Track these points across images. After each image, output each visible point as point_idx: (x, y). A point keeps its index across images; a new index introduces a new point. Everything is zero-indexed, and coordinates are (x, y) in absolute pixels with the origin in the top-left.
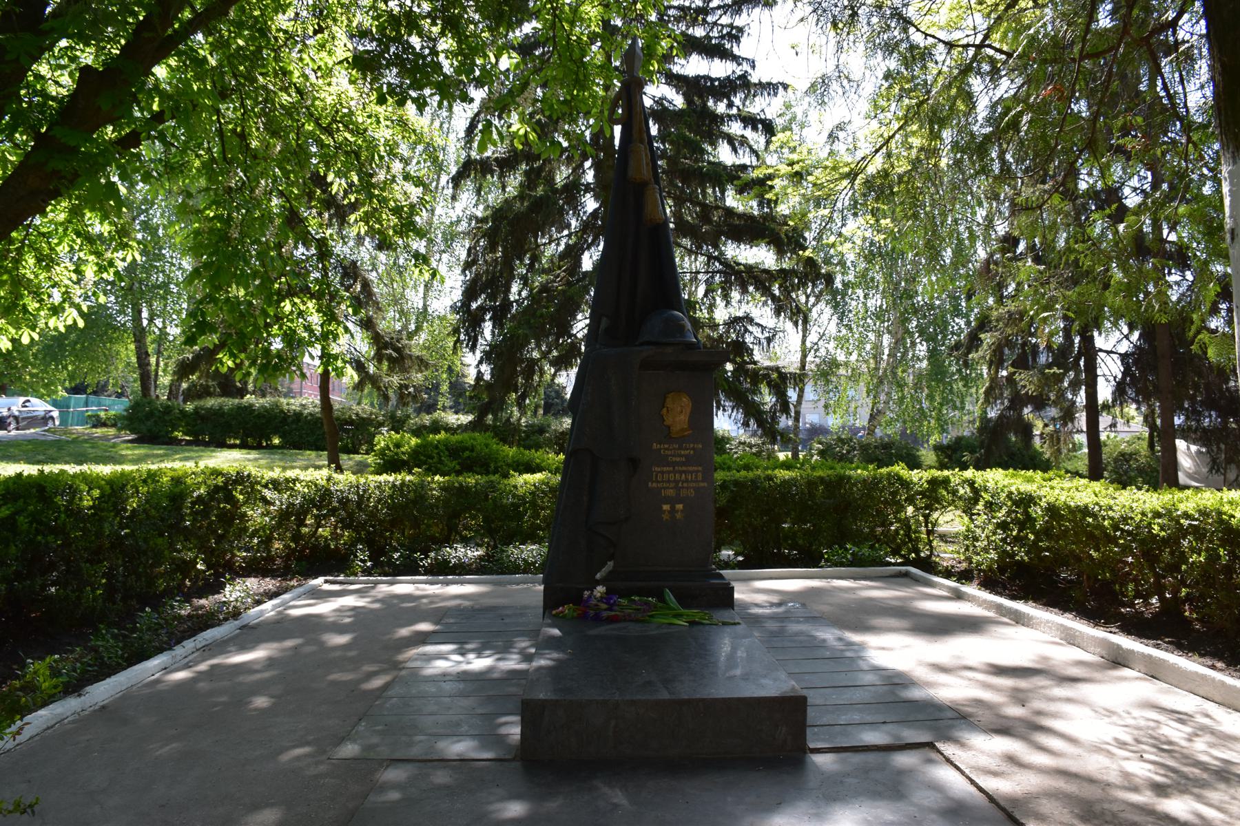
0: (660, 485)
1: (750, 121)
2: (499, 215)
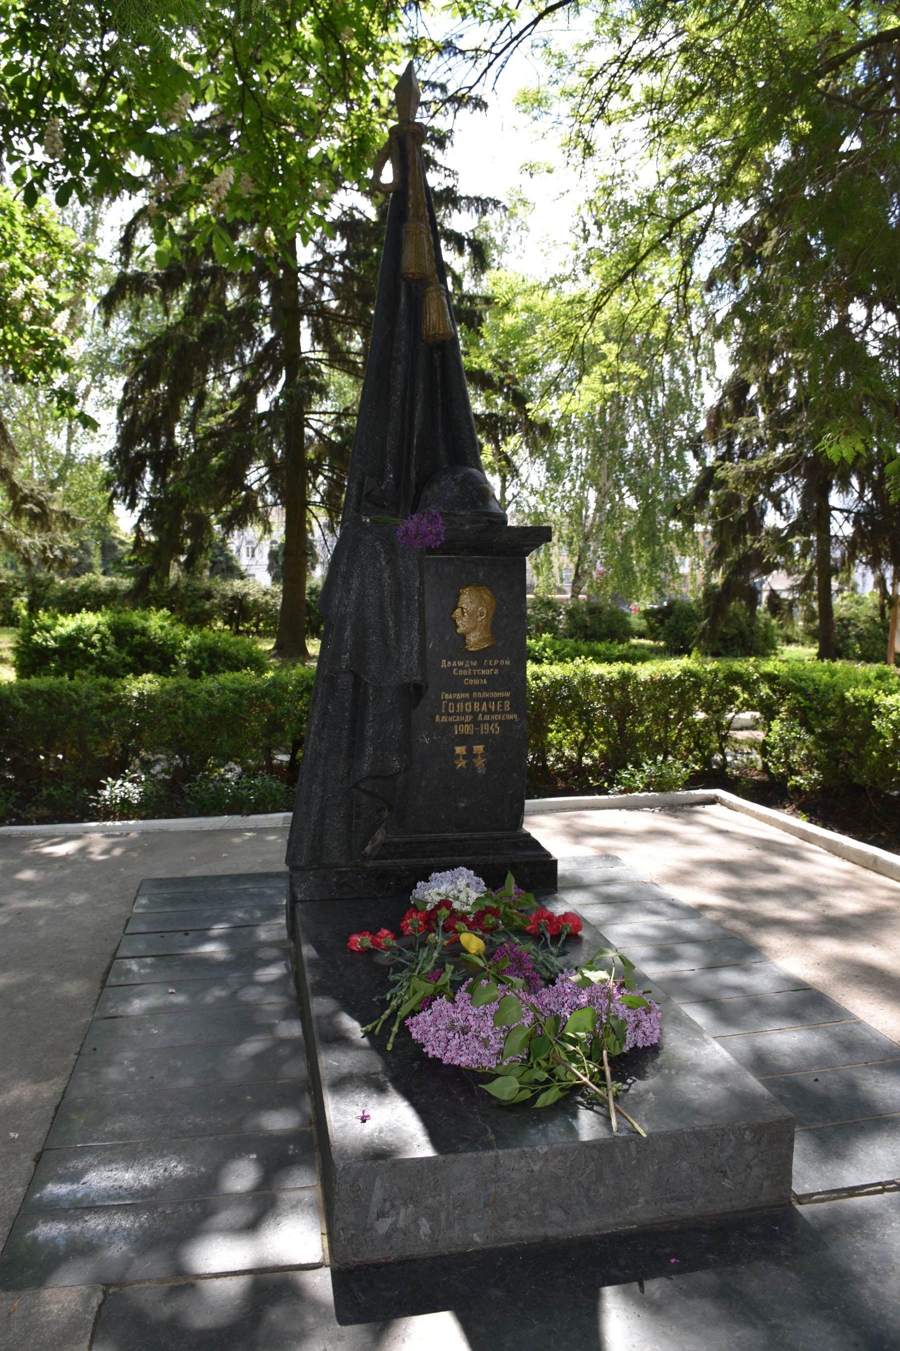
2: (160, 345)
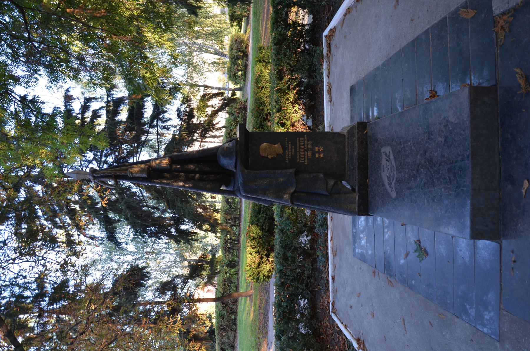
1: (85, 108)
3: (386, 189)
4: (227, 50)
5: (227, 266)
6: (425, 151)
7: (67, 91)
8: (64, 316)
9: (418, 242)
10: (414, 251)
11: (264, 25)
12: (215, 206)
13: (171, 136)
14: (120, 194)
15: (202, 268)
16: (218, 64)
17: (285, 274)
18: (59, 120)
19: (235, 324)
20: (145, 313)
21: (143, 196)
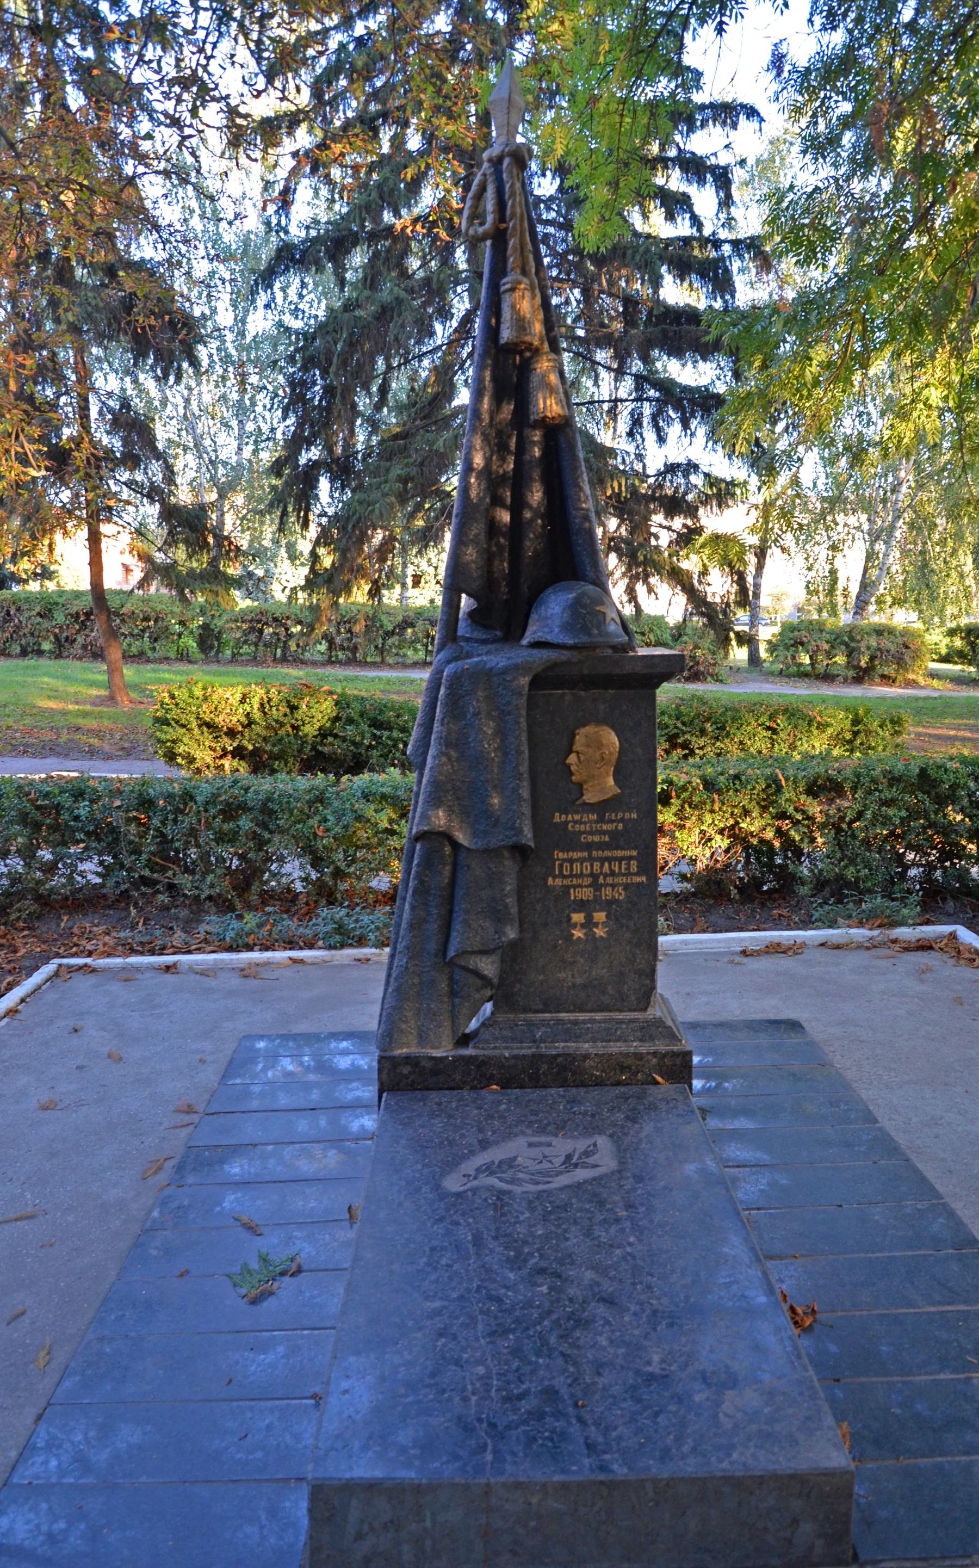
0: (567, 882)
1: (695, 167)
3: (472, 1153)
4: (874, 617)
5: (205, 627)
6: (609, 1301)
7: (752, 112)
8: (38, 108)
9: (294, 1268)
10: (264, 1251)
11: (961, 733)
12: (390, 587)
13: (608, 443)
14: (427, 281)
15: (197, 544)
16: (831, 591)
17: (182, 812)
18: (664, 86)
19: (24, 653)
20: (49, 364)
21: (420, 357)
